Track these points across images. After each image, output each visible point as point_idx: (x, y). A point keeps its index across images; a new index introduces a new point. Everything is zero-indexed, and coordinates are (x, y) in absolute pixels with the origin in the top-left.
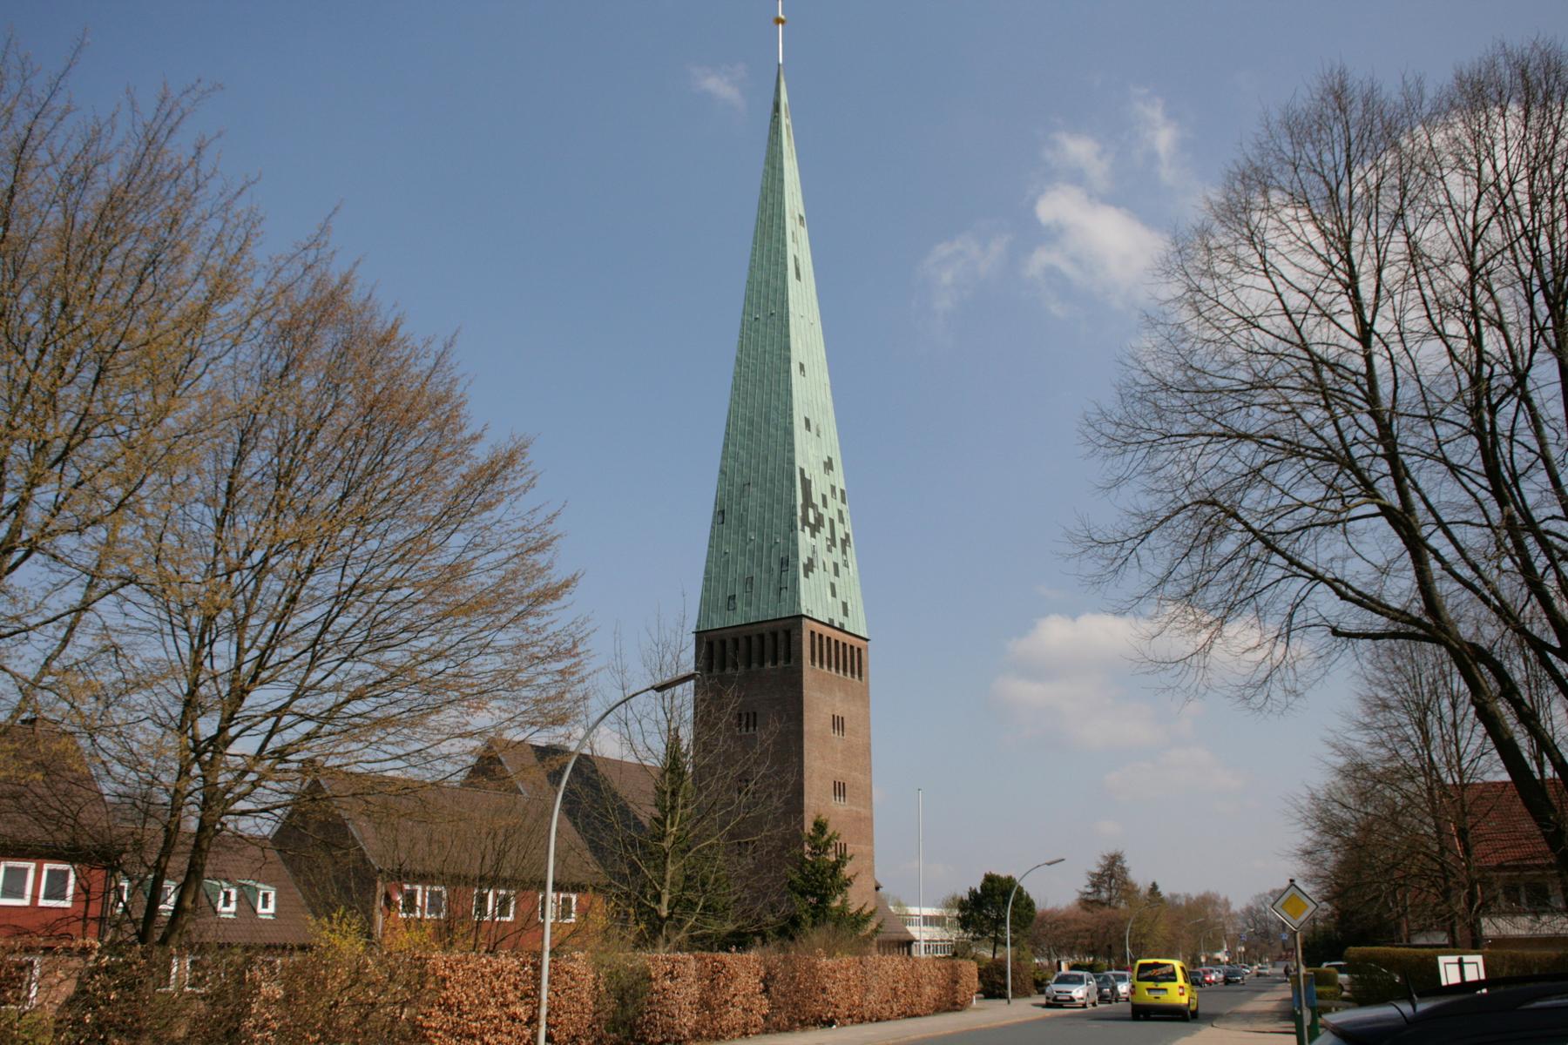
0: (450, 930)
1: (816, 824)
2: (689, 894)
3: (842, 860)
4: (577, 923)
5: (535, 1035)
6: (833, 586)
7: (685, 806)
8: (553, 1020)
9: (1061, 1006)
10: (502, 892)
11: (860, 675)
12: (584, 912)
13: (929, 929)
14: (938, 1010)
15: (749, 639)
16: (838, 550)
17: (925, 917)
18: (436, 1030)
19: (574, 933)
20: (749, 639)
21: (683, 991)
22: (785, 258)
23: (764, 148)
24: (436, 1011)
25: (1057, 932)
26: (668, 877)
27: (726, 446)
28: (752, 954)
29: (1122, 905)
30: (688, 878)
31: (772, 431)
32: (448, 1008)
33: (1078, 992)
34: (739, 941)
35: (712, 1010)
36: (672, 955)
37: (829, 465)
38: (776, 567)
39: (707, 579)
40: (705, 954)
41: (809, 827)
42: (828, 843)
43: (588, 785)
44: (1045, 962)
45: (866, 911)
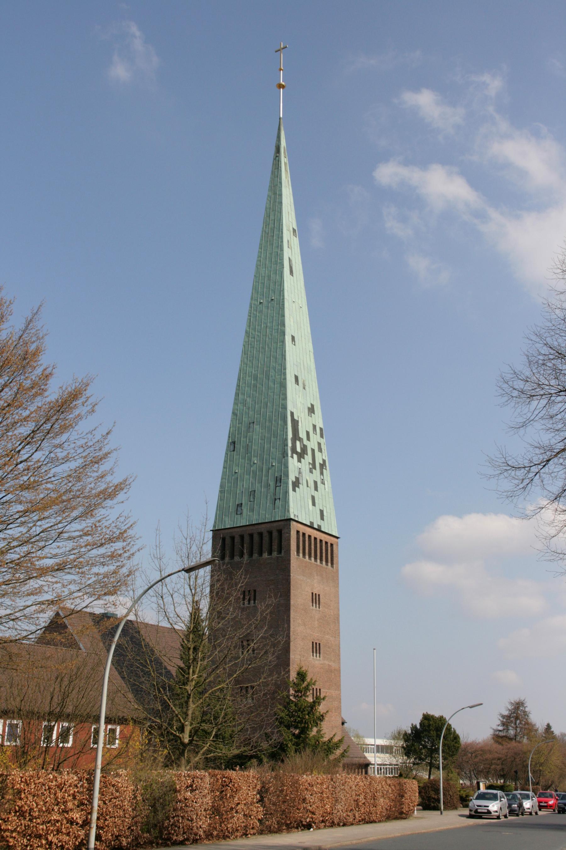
0: (24, 753)
1: (298, 674)
2: (205, 726)
3: (318, 701)
4: (120, 749)
5: (87, 835)
6: (313, 498)
7: (203, 659)
8: (101, 823)
9: (480, 817)
10: (66, 724)
11: (332, 564)
12: (126, 739)
13: (382, 755)
14: (389, 818)
15: (251, 536)
16: (317, 472)
17: (378, 746)
18: (12, 832)
19: (118, 756)
20: (251, 536)
21: (200, 800)
22: (282, 259)
23: (269, 179)
24: (12, 817)
25: (477, 760)
26: (190, 712)
27: (237, 394)
28: (252, 772)
29: (525, 740)
30: (204, 713)
31: (271, 384)
32: (21, 813)
33: (494, 806)
34: (240, 762)
35: (221, 815)
36: (192, 773)
37: (311, 410)
38: (272, 483)
39: (222, 492)
40: (217, 771)
41: (293, 676)
42: (307, 689)
43: (132, 645)
44: (468, 783)
45: (336, 739)
